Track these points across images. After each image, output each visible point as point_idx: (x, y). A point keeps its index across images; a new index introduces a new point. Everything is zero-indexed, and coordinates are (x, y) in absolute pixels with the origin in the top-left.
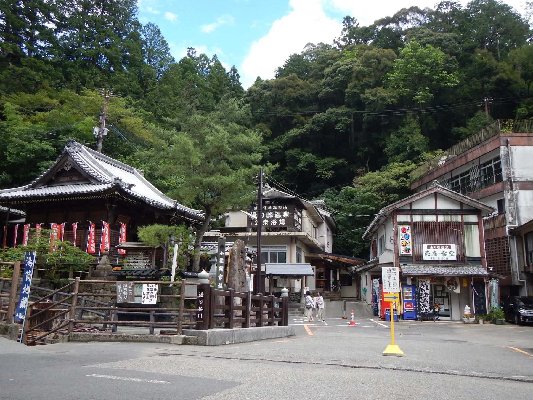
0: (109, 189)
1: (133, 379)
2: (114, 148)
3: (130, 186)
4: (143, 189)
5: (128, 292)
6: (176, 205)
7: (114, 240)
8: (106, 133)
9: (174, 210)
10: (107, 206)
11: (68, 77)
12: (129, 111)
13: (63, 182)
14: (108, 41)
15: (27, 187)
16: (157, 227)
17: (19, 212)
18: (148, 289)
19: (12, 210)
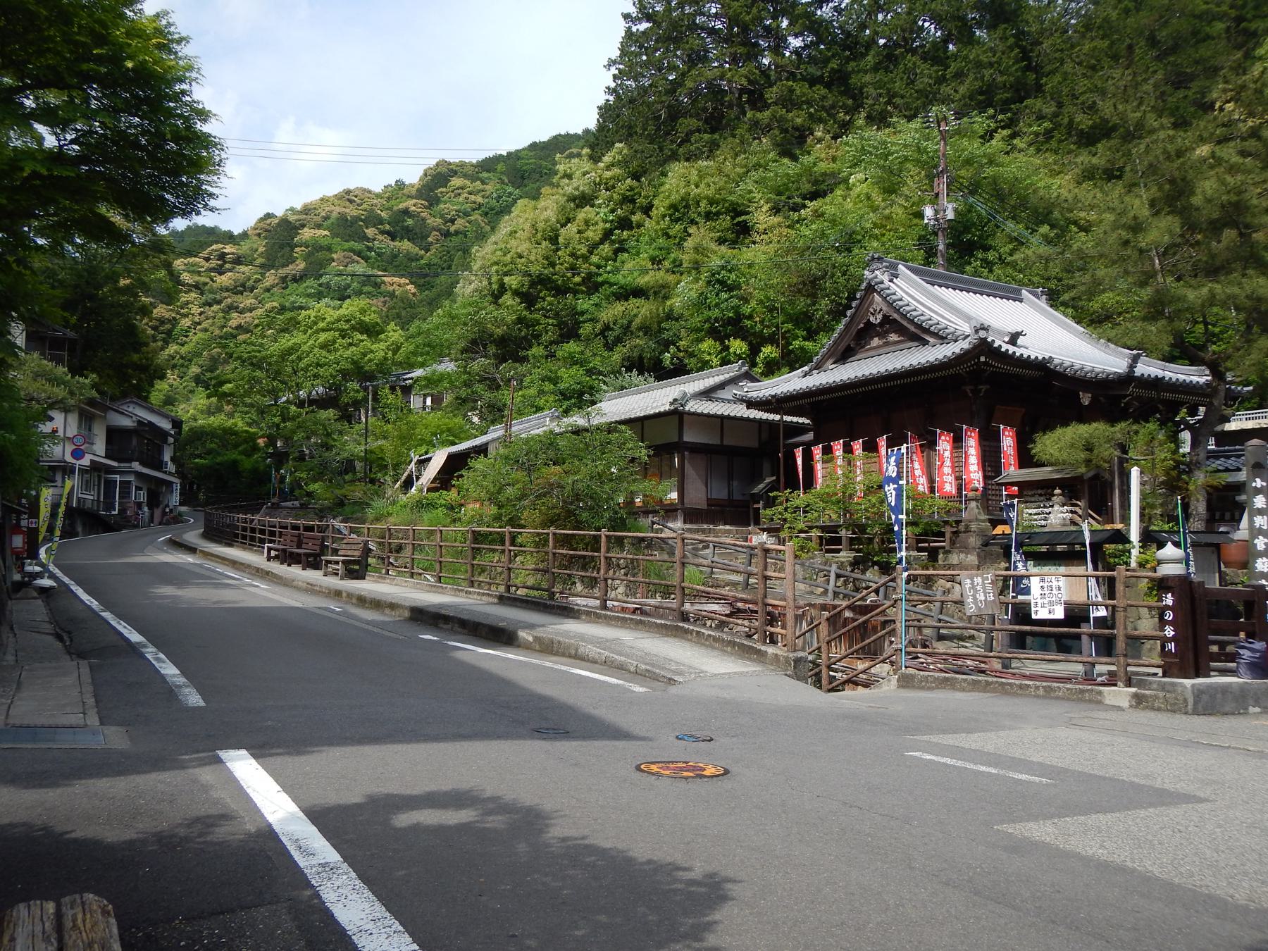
1: (983, 768)
2: (963, 253)
4: (1045, 334)
5: (985, 593)
7: (991, 461)
8: (950, 215)
9: (1128, 379)
10: (968, 389)
11: (857, 98)
14: (621, 500)
15: (806, 368)
17: (801, 420)
18: (1042, 588)
19: (788, 418)
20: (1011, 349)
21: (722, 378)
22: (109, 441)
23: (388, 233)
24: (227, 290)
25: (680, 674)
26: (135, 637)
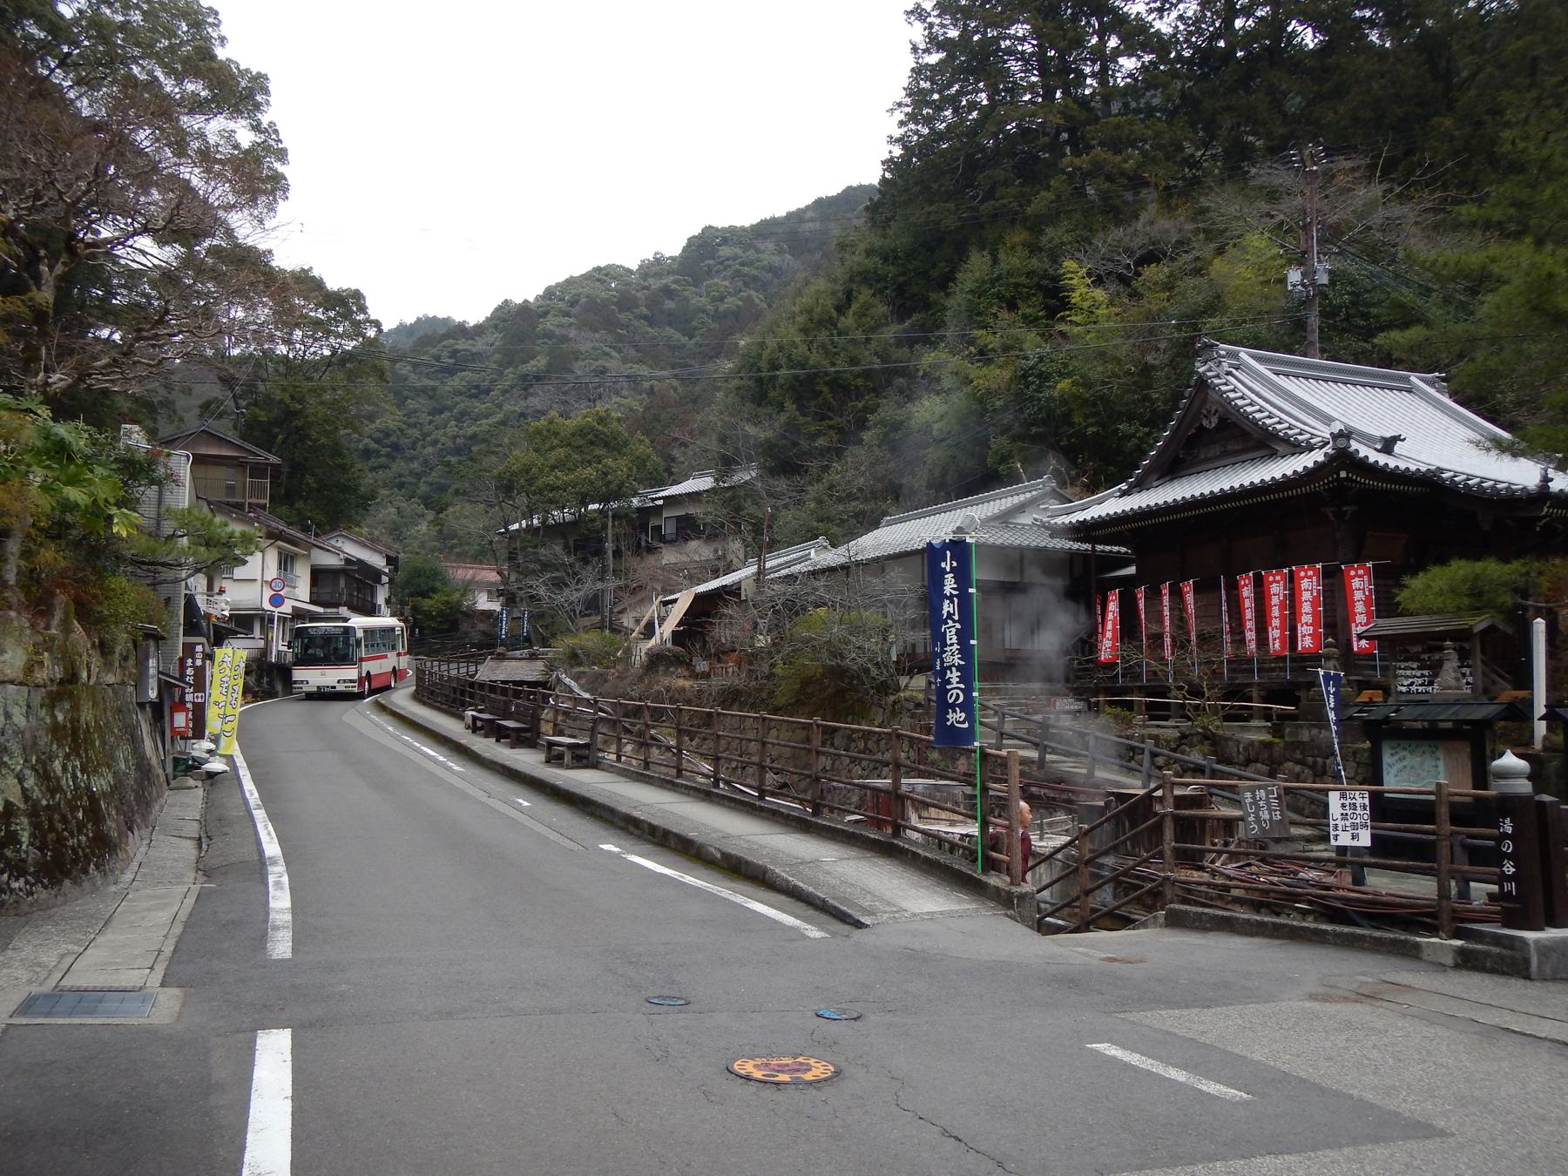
0: (1319, 468)
2: (1353, 332)
3: (1388, 445)
4: (1430, 434)
6: (1546, 480)
9: (1543, 494)
10: (1329, 511)
12: (1377, 218)
13: (1207, 460)
15: (1124, 486)
16: (1460, 569)
18: (1343, 806)
19: (1099, 547)
20: (1382, 459)
21: (1016, 500)
22: (314, 582)
23: (645, 318)
24: (461, 394)
25: (872, 913)
26: (272, 848)
